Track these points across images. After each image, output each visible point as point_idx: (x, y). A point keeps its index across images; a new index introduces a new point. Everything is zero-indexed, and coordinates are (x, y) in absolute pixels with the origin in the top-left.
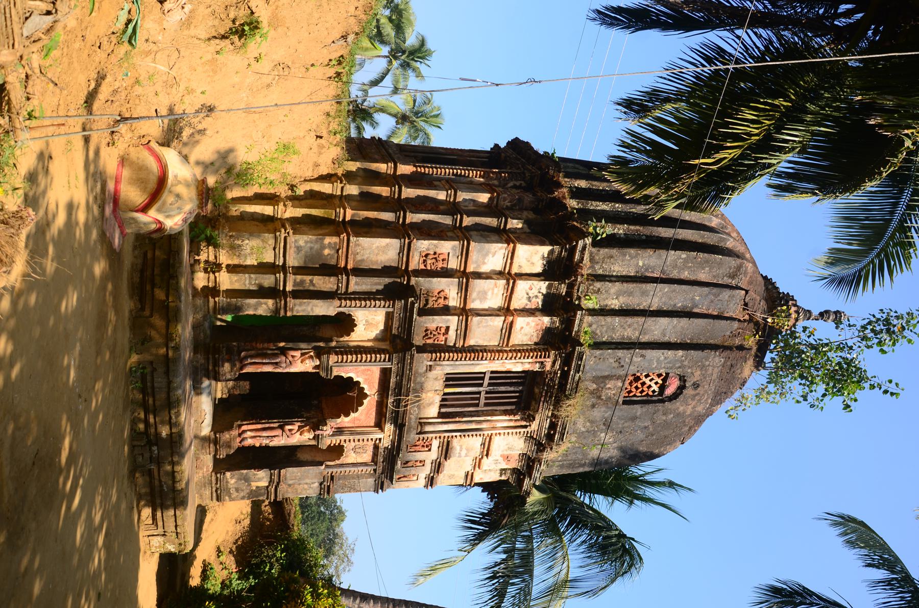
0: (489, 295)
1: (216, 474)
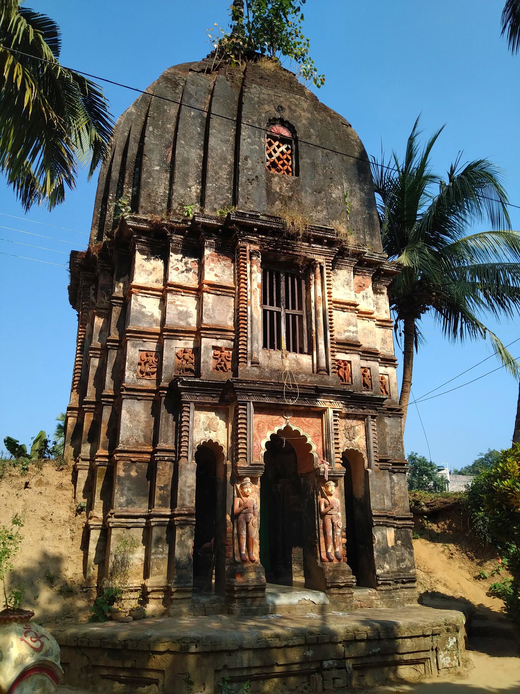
1: (378, 585)
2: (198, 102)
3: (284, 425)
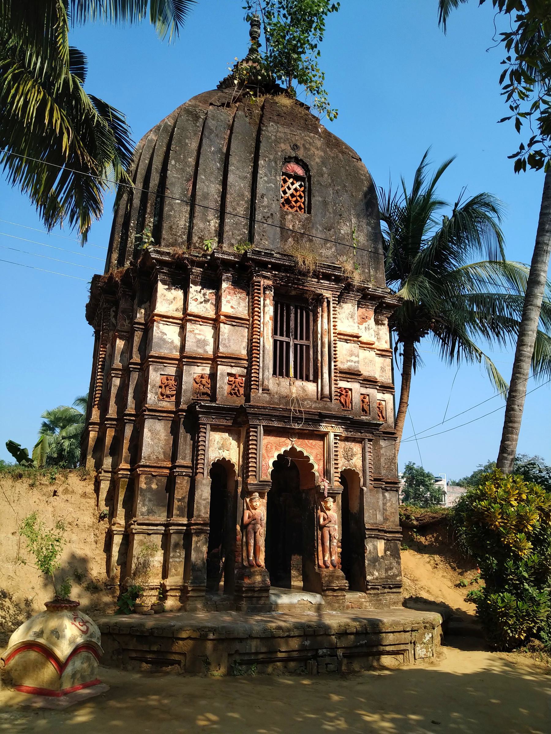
0: (201, 336)
1: (368, 589)
2: (218, 137)
3: (290, 447)
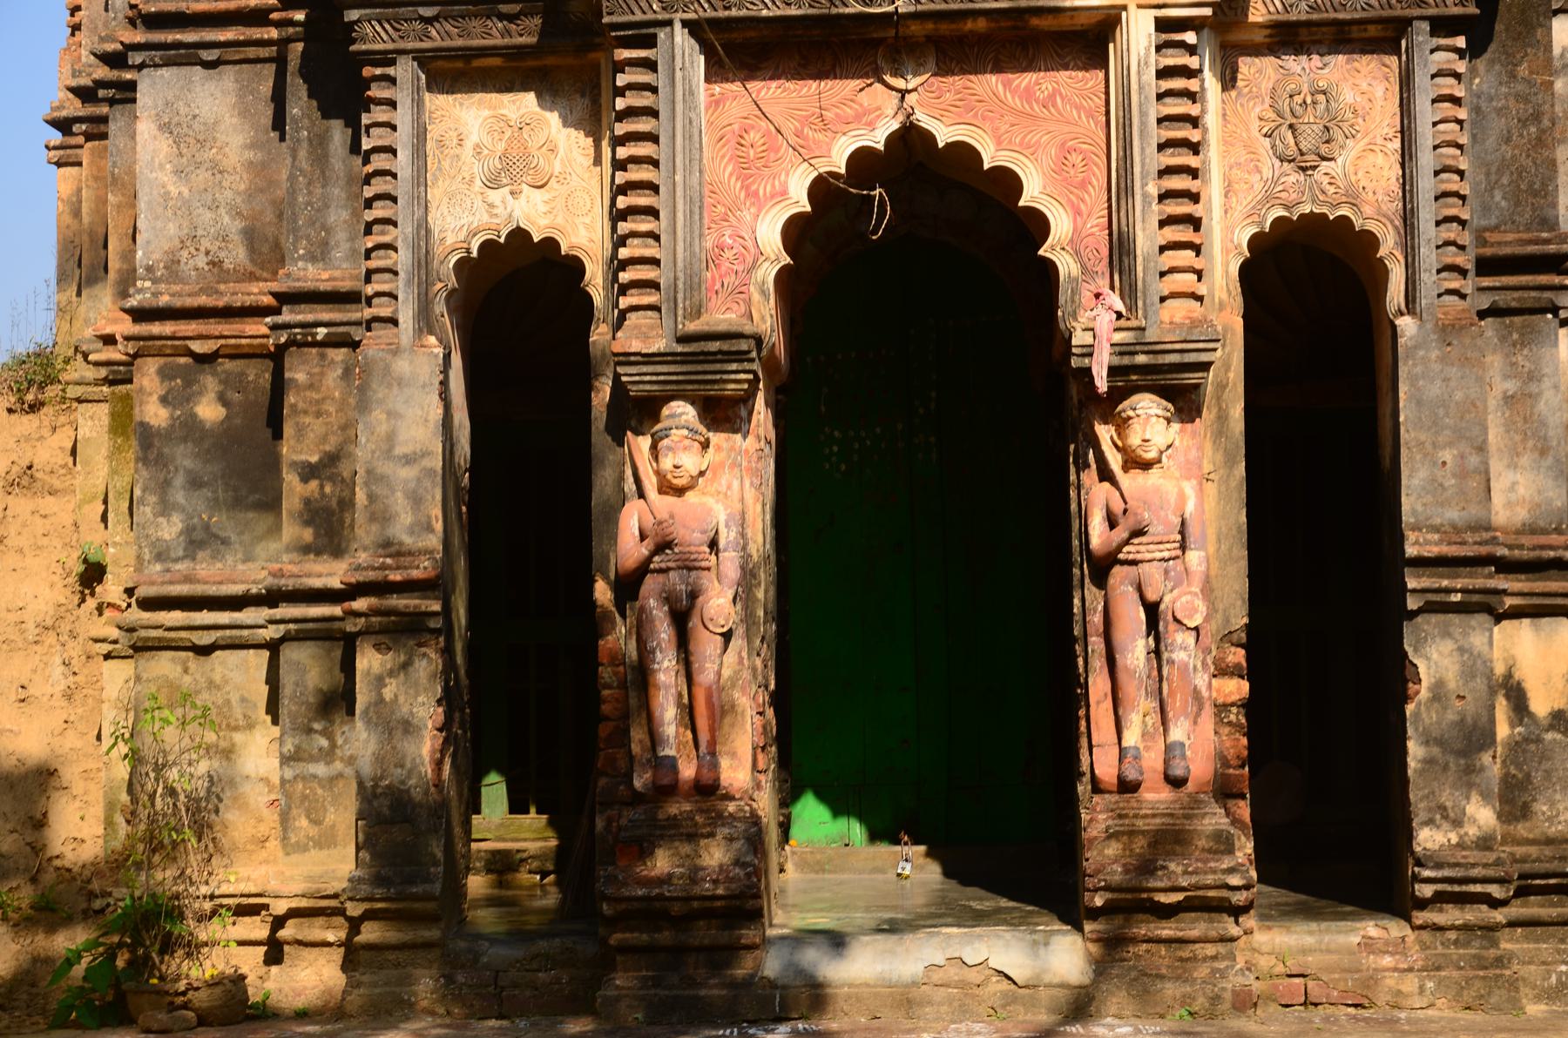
1: (1423, 904)
